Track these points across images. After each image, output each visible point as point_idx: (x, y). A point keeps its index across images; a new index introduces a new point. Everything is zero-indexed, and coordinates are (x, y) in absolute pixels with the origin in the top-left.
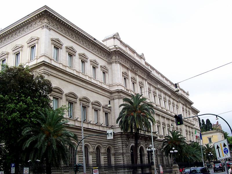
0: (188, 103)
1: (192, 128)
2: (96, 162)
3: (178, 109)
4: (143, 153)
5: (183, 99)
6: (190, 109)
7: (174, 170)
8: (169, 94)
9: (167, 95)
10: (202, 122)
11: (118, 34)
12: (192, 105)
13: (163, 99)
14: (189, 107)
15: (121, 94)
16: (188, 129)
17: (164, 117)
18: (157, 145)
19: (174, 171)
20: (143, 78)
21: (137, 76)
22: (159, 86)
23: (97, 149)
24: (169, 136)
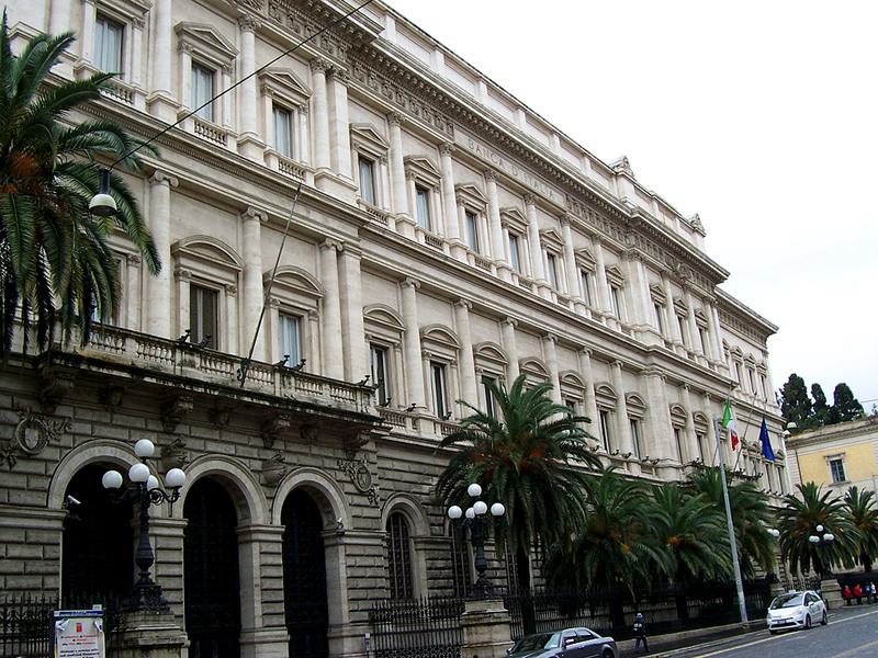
0: (689, 271)
1: (720, 401)
2: (391, 578)
3: (622, 295)
4: (246, 522)
5: (659, 241)
6: (712, 303)
7: (475, 638)
8: (558, 199)
9: (497, 179)
10: (815, 396)
11: (626, 162)
12: (718, 286)
13: (672, 306)
14: (706, 294)
15: (655, 360)
16: (691, 404)
17: (701, 393)
18: (414, 478)
19: (471, 647)
20: (592, 236)
21: (568, 228)
22: (462, 139)
23: (396, 523)
24: (489, 420)
